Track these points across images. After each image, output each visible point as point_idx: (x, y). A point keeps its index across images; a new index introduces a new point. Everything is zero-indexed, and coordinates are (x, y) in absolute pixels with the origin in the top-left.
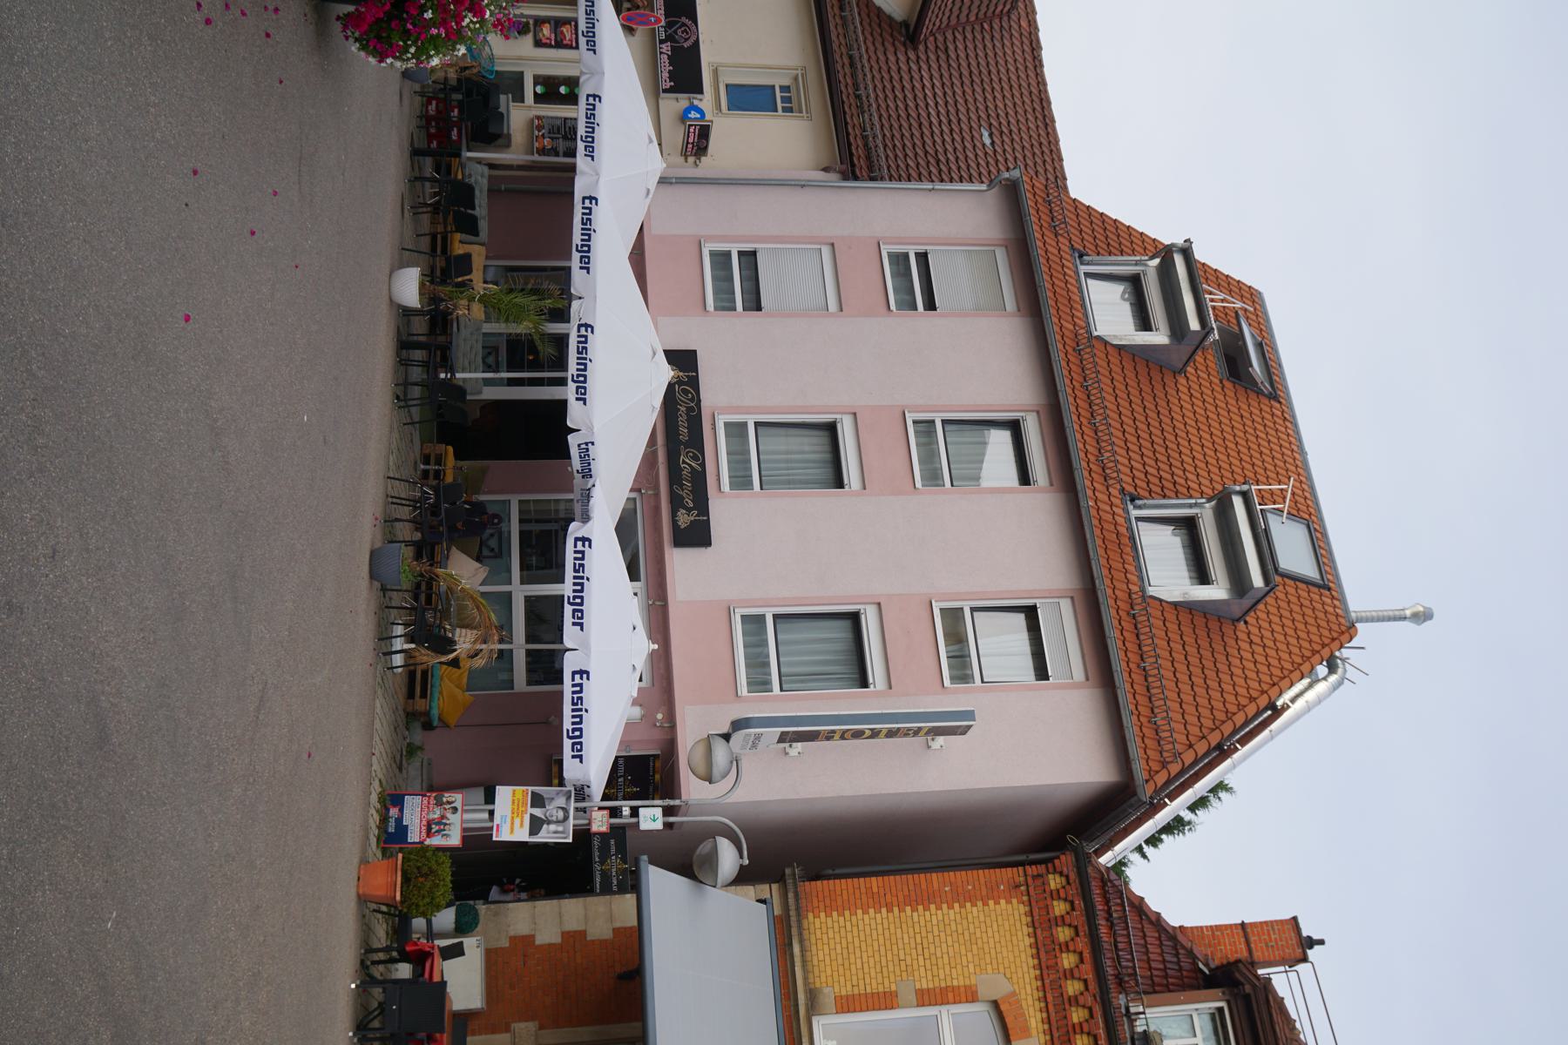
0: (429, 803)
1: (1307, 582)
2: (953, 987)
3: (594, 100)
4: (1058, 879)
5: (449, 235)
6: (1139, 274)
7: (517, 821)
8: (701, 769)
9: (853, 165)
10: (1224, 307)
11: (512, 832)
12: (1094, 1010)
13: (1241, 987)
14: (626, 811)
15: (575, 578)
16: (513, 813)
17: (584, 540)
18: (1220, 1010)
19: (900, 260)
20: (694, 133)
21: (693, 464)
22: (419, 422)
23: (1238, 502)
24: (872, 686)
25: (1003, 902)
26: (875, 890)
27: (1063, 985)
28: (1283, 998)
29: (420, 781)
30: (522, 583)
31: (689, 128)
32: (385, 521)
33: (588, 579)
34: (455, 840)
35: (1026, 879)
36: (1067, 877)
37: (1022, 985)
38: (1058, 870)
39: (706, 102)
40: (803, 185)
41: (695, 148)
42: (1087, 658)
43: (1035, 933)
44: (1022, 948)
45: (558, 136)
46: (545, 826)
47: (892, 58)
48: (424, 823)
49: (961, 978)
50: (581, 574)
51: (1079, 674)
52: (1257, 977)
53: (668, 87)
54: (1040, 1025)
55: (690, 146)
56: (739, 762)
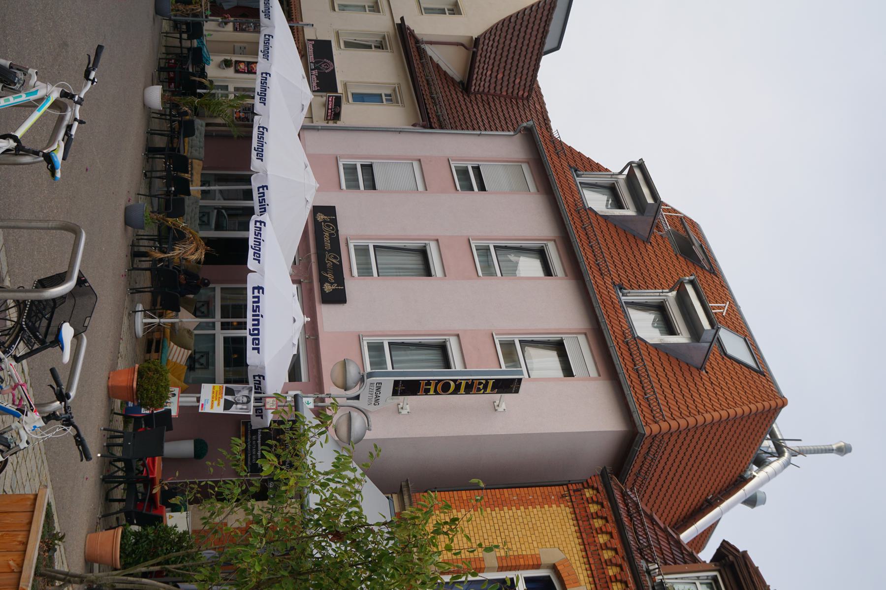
1: (748, 367)
2: (523, 555)
3: (261, 225)
4: (591, 491)
6: (614, 183)
7: (216, 403)
8: (340, 381)
10: (671, 216)
11: (212, 407)
12: (623, 567)
13: (727, 558)
15: (253, 315)
17: (261, 222)
18: (715, 579)
23: (689, 289)
25: (554, 506)
26: (465, 498)
27: (601, 554)
28: (758, 567)
33: (262, 316)
35: (569, 493)
36: (597, 490)
37: (571, 554)
40: (400, 131)
43: (578, 523)
44: (570, 532)
46: (234, 405)
49: (528, 550)
50: (258, 313)
51: (593, 373)
54: (586, 578)
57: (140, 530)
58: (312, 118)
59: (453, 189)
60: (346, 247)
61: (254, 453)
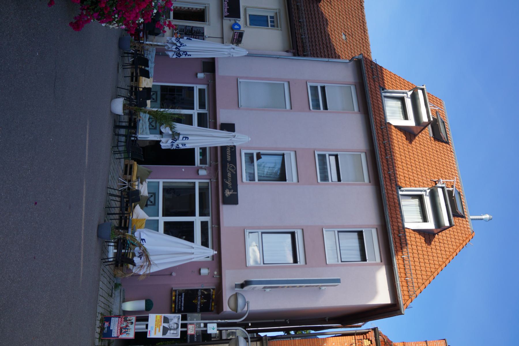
0: (121, 320)
5: (138, 77)
7: (157, 329)
9: (298, 50)
11: (155, 334)
14: (202, 325)
16: (156, 326)
19: (314, 89)
20: (237, 35)
21: (232, 171)
22: (124, 158)
24: (299, 263)
29: (120, 298)
30: (163, 216)
31: (235, 33)
32: (106, 208)
34: (131, 336)
36: (371, 341)
38: (368, 338)
39: (241, 22)
41: (237, 41)
42: (382, 253)
45: (183, 33)
46: (169, 331)
47: (312, 6)
48: (119, 328)
51: (378, 260)
52: (229, 13)
53: (227, 15)
55: (235, 40)
56: (248, 304)
57: (127, 125)
58: (223, 38)
59: (308, 109)
60: (240, 157)
61: (180, 304)
